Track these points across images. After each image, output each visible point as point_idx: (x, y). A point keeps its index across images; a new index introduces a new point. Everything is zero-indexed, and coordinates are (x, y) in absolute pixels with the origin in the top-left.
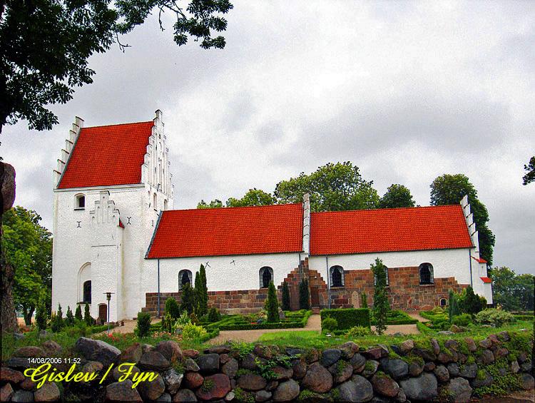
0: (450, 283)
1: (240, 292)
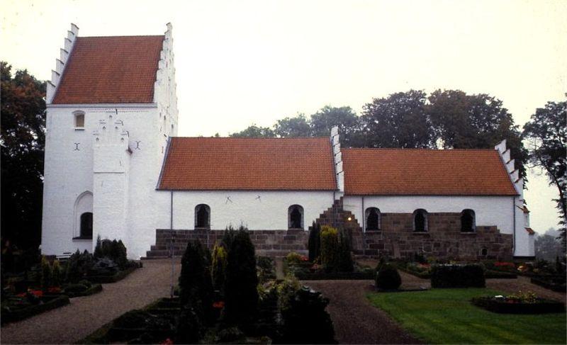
0: (493, 232)
1: (265, 232)
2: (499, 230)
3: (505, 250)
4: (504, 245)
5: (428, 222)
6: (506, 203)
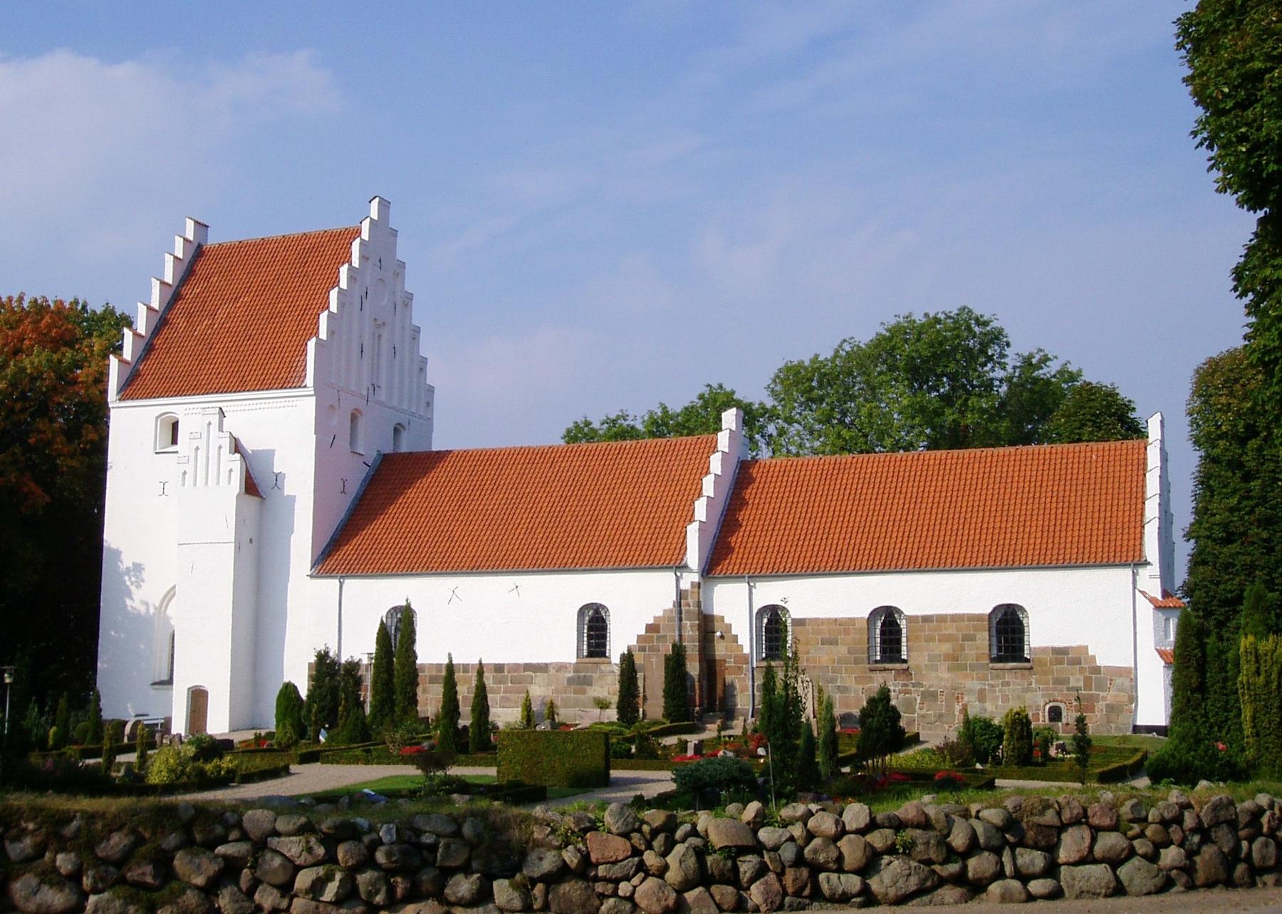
0: (1073, 662)
1: (528, 667)
2: (1094, 657)
3: (1111, 708)
4: (1110, 696)
5: (907, 641)
6: (689, 744)
